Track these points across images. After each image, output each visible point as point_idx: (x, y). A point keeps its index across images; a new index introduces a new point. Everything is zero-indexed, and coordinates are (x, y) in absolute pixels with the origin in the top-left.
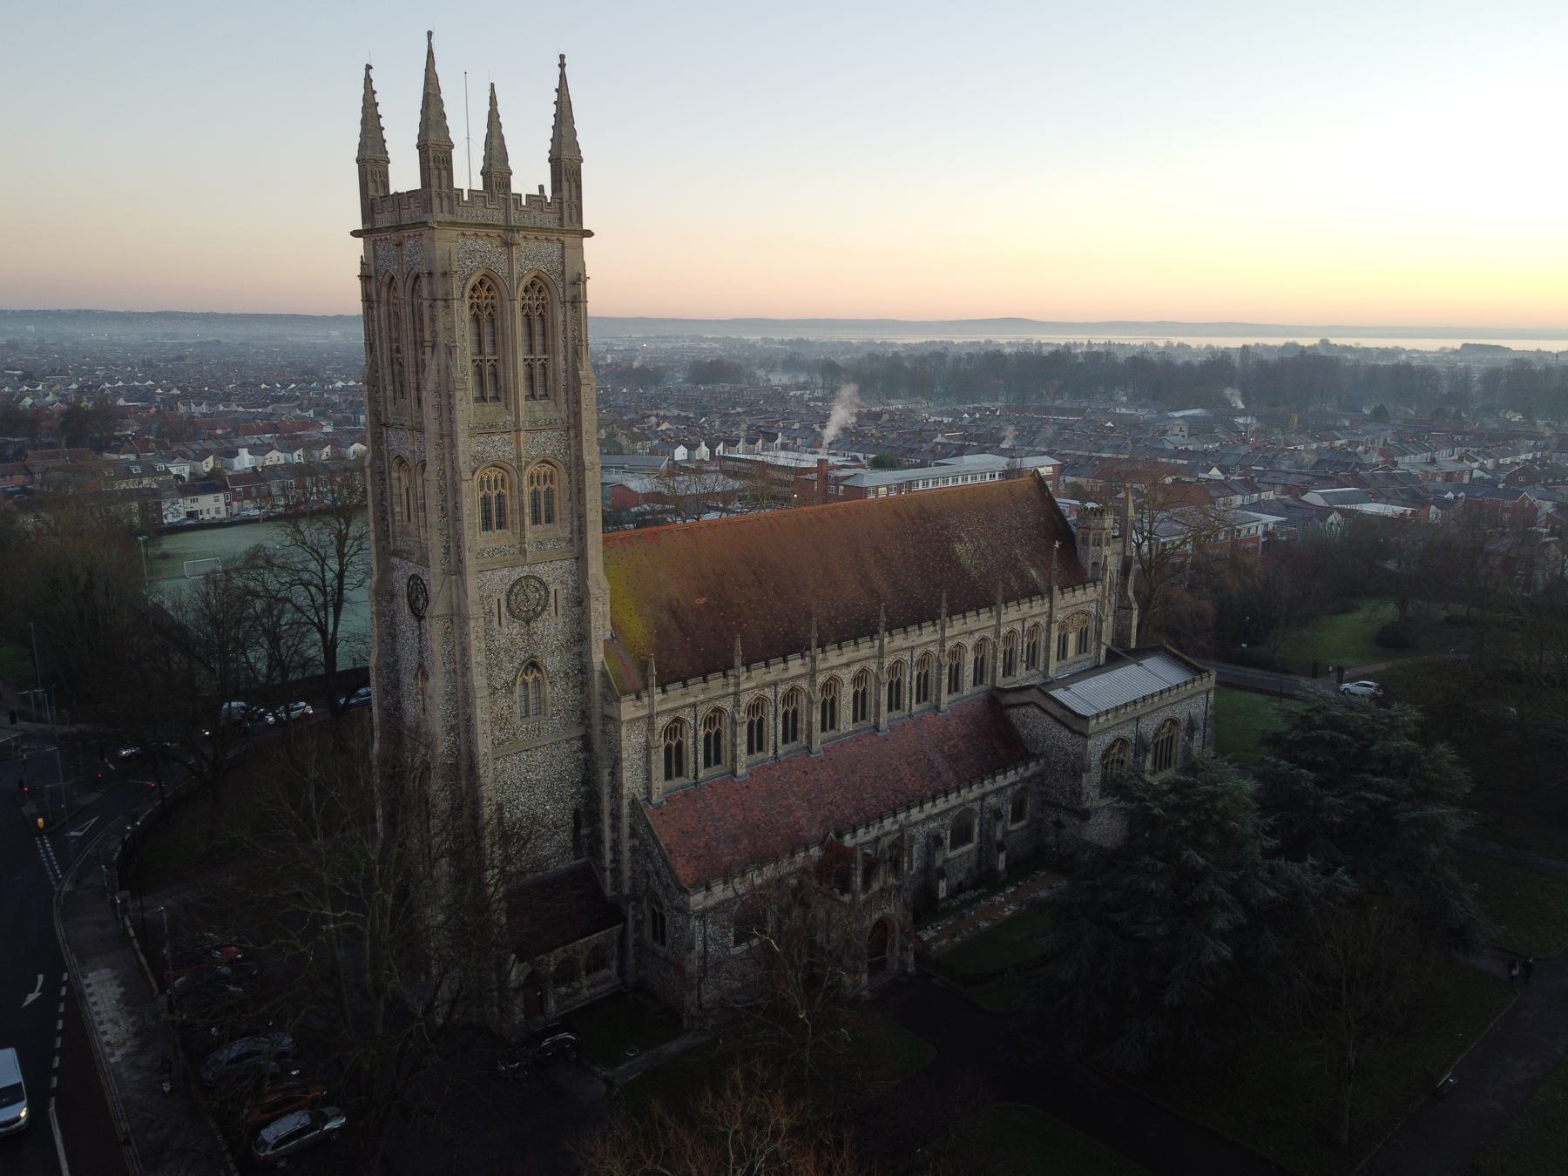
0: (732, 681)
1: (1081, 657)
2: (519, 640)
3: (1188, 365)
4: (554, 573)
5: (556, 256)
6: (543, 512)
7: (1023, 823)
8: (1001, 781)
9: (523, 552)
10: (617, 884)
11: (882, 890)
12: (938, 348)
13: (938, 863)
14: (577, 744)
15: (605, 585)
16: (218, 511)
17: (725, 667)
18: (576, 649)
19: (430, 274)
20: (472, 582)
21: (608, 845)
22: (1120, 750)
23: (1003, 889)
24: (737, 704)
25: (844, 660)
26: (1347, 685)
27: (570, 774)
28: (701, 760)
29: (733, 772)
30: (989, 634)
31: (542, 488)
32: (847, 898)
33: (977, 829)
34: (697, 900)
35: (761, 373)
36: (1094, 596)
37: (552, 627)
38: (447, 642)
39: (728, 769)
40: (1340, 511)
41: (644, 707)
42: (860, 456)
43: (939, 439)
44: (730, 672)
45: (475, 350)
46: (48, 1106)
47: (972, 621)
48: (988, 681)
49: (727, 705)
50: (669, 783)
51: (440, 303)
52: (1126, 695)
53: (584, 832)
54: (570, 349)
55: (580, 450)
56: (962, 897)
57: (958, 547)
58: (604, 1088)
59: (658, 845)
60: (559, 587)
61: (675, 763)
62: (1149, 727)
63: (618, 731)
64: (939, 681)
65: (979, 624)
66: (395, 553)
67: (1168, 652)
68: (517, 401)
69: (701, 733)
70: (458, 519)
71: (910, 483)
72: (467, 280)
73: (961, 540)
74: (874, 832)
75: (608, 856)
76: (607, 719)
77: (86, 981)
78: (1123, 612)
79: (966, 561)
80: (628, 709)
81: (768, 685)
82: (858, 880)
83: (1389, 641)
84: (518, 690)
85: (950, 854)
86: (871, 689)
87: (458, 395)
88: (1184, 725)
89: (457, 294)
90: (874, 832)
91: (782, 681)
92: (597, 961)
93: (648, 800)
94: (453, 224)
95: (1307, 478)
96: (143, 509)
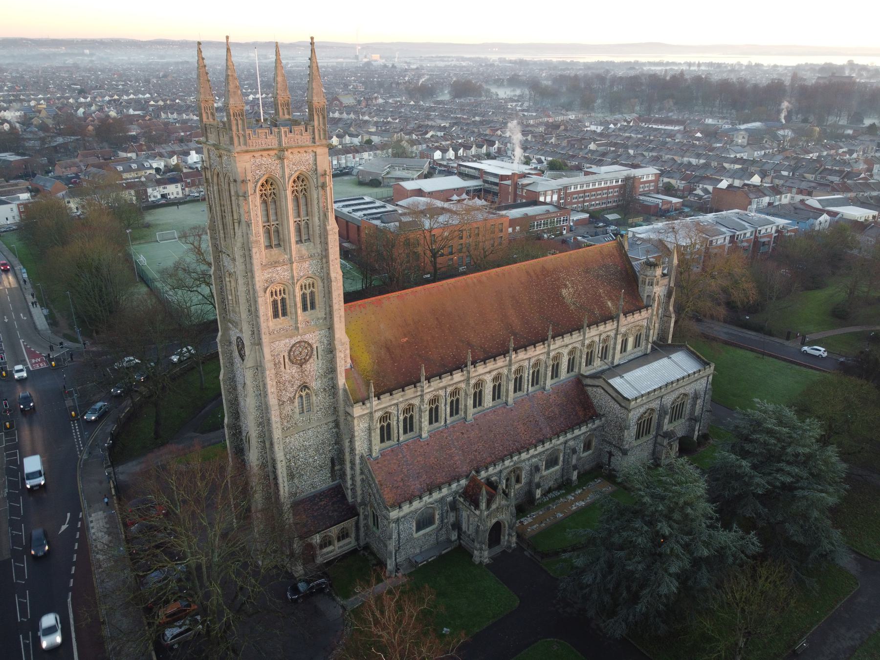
0: (419, 389)
1: (636, 350)
2: (296, 375)
3: (756, 86)
4: (315, 338)
5: (311, 161)
6: (308, 304)
7: (590, 452)
8: (577, 432)
9: (297, 328)
10: (354, 496)
11: (497, 508)
12: (601, 71)
13: (537, 480)
14: (332, 425)
15: (346, 339)
16: (178, 194)
17: (415, 382)
18: (330, 376)
19: (235, 181)
20: (267, 351)
21: (349, 477)
22: (650, 414)
23: (574, 491)
24: (422, 401)
25: (487, 370)
26: (805, 348)
27: (328, 440)
28: (401, 431)
29: (420, 436)
30: (578, 345)
31: (308, 292)
32: (477, 512)
33: (561, 458)
34: (394, 514)
35: (494, 90)
36: (646, 316)
37: (314, 367)
38: (255, 380)
39: (418, 434)
40: (829, 213)
41: (367, 408)
42: (543, 158)
43: (592, 146)
44: (418, 385)
45: (265, 219)
46: (67, 598)
47: (567, 339)
48: (576, 370)
49: (416, 402)
50: (383, 445)
51: (241, 198)
52: (658, 378)
53: (337, 468)
54: (322, 214)
55: (329, 270)
56: (550, 495)
57: (564, 292)
58: (341, 611)
59: (374, 483)
60: (319, 345)
61: (386, 434)
62: (668, 400)
63: (353, 421)
64: (546, 374)
65: (573, 340)
66: (230, 321)
67: (688, 349)
68: (290, 247)
69: (401, 418)
70: (257, 317)
71: (566, 188)
72: (257, 182)
73: (566, 286)
74: (499, 468)
75: (349, 482)
76: (347, 414)
77: (91, 519)
78: (665, 319)
79: (569, 300)
80: (358, 411)
81: (441, 388)
82: (483, 505)
83: (839, 315)
84: (296, 401)
85: (544, 473)
86: (504, 383)
87: (254, 250)
88: (691, 396)
89: (250, 191)
90: (499, 468)
91: (449, 385)
92: (343, 535)
93: (371, 455)
94: (247, 152)
95: (813, 184)
96: (137, 194)
